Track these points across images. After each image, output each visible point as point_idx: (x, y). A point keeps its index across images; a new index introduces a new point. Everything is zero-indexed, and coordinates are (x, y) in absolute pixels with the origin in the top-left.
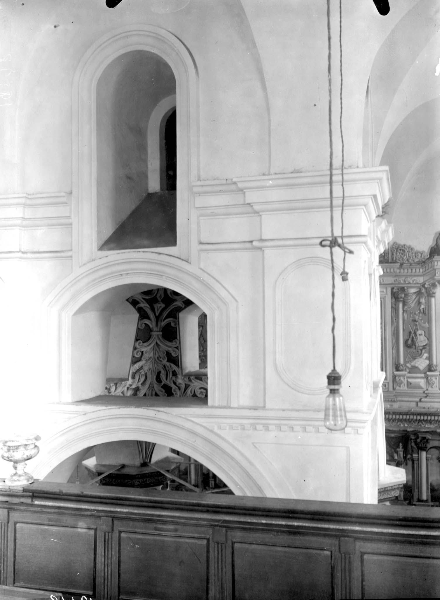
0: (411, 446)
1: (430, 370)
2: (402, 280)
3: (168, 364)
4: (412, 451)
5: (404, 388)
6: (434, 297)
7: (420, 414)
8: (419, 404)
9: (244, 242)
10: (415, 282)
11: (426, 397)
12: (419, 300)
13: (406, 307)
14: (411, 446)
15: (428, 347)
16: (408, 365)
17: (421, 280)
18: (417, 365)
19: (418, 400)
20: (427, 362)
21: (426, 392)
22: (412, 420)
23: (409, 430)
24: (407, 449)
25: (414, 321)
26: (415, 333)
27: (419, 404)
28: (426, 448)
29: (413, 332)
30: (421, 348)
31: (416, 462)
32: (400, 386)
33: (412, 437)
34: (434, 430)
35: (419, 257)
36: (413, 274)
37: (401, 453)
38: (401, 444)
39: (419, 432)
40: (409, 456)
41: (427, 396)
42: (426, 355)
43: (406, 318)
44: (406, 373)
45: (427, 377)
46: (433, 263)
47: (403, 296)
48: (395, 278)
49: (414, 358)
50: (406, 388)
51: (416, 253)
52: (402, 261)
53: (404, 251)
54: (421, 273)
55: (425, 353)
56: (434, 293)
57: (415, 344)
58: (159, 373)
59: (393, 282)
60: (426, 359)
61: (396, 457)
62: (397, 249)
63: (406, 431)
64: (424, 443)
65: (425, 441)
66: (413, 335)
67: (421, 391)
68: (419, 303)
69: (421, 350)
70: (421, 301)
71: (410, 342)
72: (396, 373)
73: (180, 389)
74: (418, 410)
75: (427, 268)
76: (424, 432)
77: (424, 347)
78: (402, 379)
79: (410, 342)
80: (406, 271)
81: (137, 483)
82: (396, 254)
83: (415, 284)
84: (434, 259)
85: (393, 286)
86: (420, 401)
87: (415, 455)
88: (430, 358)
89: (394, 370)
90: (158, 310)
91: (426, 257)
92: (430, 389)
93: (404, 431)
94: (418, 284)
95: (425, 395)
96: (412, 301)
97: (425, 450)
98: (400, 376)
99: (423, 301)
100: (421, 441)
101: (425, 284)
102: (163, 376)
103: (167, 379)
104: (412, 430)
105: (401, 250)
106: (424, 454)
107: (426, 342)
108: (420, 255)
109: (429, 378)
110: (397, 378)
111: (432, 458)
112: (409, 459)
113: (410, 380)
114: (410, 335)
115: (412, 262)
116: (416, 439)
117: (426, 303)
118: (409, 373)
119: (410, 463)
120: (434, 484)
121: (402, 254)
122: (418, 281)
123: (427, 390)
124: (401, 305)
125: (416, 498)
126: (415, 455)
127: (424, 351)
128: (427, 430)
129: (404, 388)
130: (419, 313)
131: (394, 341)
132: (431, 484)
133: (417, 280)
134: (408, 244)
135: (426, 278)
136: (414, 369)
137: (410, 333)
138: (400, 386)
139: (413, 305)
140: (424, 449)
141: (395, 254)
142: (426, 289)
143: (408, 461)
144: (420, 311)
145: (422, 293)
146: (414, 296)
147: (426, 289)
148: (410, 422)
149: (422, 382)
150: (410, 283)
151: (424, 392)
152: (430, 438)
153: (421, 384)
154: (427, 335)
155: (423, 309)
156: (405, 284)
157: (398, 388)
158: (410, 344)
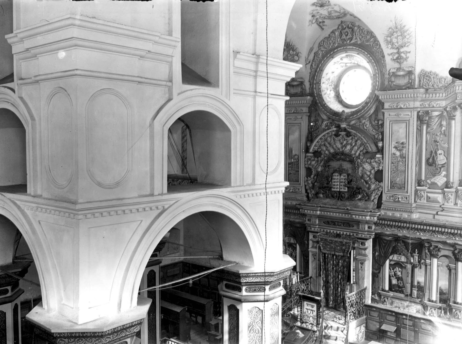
0: (425, 253)
1: (447, 187)
2: (426, 104)
4: (426, 257)
5: (424, 201)
6: (454, 119)
7: (436, 226)
8: (436, 216)
9: (229, 74)
10: (438, 106)
11: (442, 211)
12: (441, 122)
13: (429, 129)
14: (425, 253)
15: (446, 166)
16: (428, 181)
17: (443, 104)
18: (436, 181)
19: (435, 213)
20: (445, 179)
21: (442, 206)
22: (444, 232)
23: (423, 238)
24: (421, 254)
25: (436, 141)
26: (436, 153)
27: (436, 216)
28: (438, 255)
29: (434, 152)
30: (440, 166)
31: (428, 267)
32: (420, 200)
33: (427, 245)
34: (444, 240)
35: (443, 82)
36: (436, 98)
37: (417, 258)
38: (417, 250)
39: (432, 241)
40: (423, 261)
41: (443, 210)
42: (444, 173)
43: (428, 138)
44: (426, 188)
45: (444, 193)
46: (455, 87)
47: (427, 118)
48: (421, 103)
49: (434, 176)
50: (425, 201)
51: (440, 79)
52: (428, 87)
53: (430, 77)
54: (444, 97)
55: (443, 171)
56: (455, 116)
57: (435, 162)
60: (444, 177)
61: (412, 261)
62: (424, 76)
63: (421, 239)
64: (436, 251)
65: (437, 249)
66: (433, 154)
67: (438, 205)
68: (441, 125)
69: (440, 168)
70: (443, 123)
71: (431, 160)
72: (418, 187)
74: (434, 222)
75: (449, 93)
76: (436, 242)
77: (443, 166)
78: (422, 193)
79: (431, 160)
80: (431, 95)
82: (423, 80)
83: (438, 107)
84: (456, 84)
85: (419, 109)
86: (437, 214)
87: (428, 261)
88: (447, 176)
89: (417, 185)
91: (449, 82)
92: (446, 204)
93: (419, 238)
94: (440, 107)
95: (441, 209)
96: (435, 123)
97: (437, 258)
98: (421, 190)
99: (444, 123)
100: (434, 249)
101: (447, 107)
104: (426, 238)
105: (427, 76)
106: (435, 261)
107: (445, 161)
108: (443, 80)
109: (446, 194)
110: (418, 192)
111: (442, 266)
112: (422, 264)
113: (429, 195)
114: (431, 155)
115: (437, 87)
116: (429, 247)
117: (447, 125)
118: (429, 188)
119: (423, 267)
120: (443, 288)
121: (428, 80)
122: (441, 105)
123: (443, 204)
124: (425, 127)
125: (452, 299)
126: (428, 261)
127: (442, 169)
128: (439, 240)
129: (424, 201)
130: (440, 134)
131: (418, 159)
132: (440, 288)
134: (433, 71)
135: (448, 102)
136: (433, 185)
137: (432, 152)
138: (420, 200)
139: (435, 127)
140: (435, 256)
141: (422, 80)
142: (447, 112)
143: (422, 265)
144: (441, 132)
145: (444, 116)
146: (437, 119)
147: (447, 112)
148: (425, 232)
149: (440, 197)
150: (433, 107)
151: (440, 206)
152: (442, 247)
153: (438, 199)
154: (446, 155)
155: (444, 130)
156: (429, 108)
157: (418, 201)
158: (431, 162)
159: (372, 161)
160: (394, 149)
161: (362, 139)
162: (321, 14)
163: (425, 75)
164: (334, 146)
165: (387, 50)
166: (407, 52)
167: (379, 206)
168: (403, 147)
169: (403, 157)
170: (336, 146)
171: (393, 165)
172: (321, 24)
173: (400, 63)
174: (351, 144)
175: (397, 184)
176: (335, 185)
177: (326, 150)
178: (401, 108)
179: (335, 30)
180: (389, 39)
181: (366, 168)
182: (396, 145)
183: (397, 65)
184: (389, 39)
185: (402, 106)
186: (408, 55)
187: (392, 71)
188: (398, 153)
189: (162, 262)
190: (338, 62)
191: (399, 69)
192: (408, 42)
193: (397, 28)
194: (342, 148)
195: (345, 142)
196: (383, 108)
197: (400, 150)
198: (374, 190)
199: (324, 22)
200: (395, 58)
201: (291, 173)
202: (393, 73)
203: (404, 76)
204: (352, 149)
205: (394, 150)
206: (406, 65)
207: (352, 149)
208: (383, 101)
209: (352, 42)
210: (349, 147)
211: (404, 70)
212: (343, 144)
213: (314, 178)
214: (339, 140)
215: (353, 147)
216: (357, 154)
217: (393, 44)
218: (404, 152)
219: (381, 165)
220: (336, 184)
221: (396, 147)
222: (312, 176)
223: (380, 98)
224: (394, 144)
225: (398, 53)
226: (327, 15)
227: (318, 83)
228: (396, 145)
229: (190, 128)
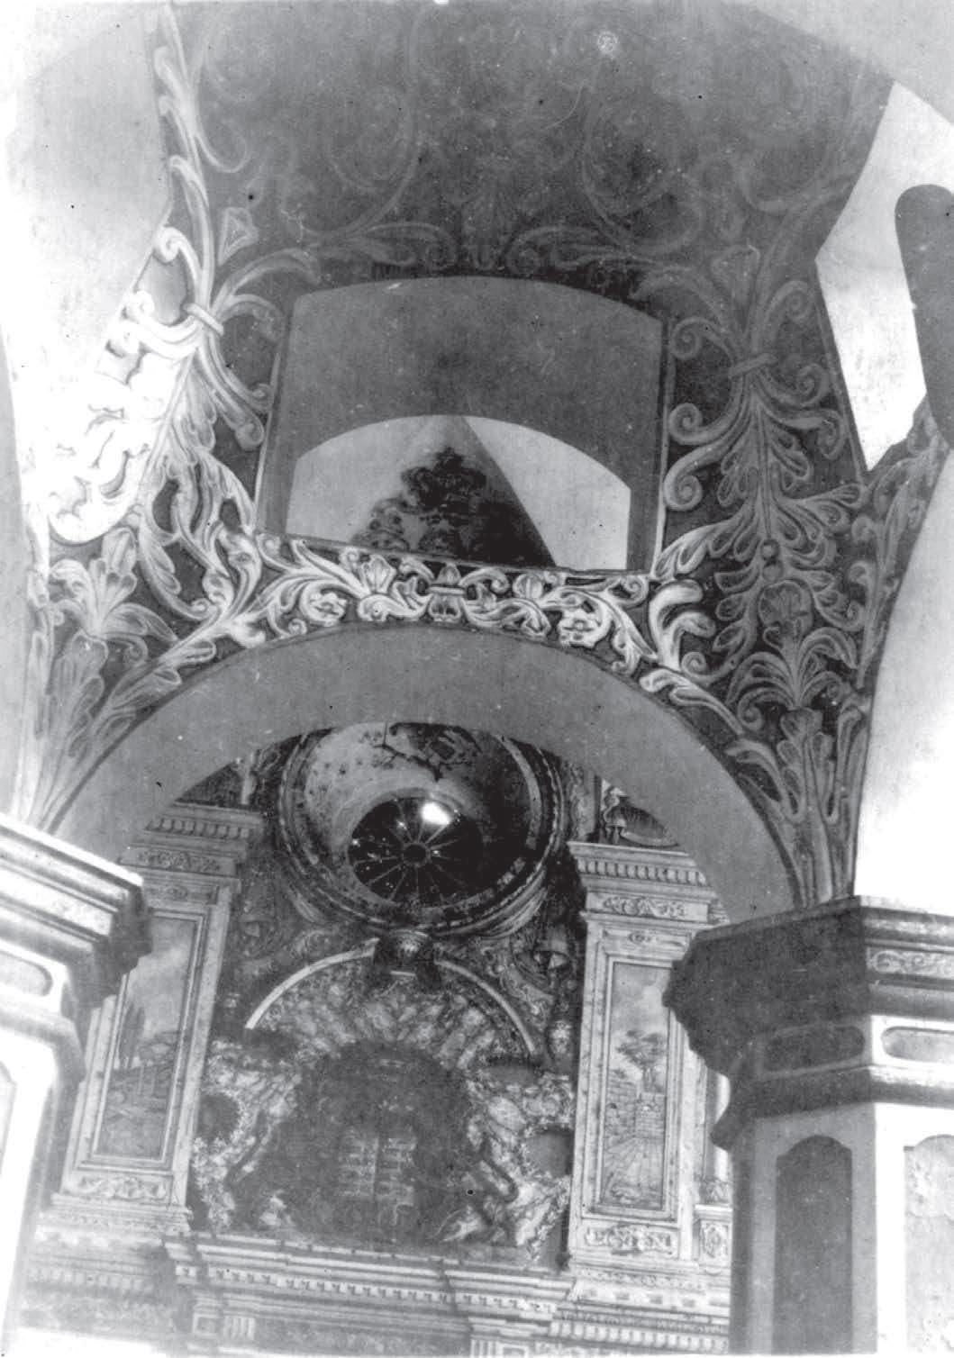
3: (213, 465)
58: (172, 487)
59: (475, 734)
72: (701, 1208)
73: (236, 586)
81: (835, 373)
89: (698, 1198)
90: (230, 242)
102: (183, 511)
103: (194, 526)
133: (531, 1219)
138: (712, 1256)
160: (621, 1056)
164: (360, 1022)
167: (560, 1259)
168: (654, 1052)
171: (612, 1112)
175: (627, 1185)
178: (649, 916)
181: (500, 1119)
182: (629, 1041)
185: (656, 913)
188: (635, 1074)
189: (389, 486)
194: (395, 1031)
197: (644, 1064)
201: (118, 1117)
205: (619, 1061)
212: (403, 1018)
213: (242, 1142)
216: (463, 1061)
218: (660, 1068)
219: (569, 1110)
220: (360, 1171)
221: (627, 1051)
222: (236, 1135)
228: (629, 1041)
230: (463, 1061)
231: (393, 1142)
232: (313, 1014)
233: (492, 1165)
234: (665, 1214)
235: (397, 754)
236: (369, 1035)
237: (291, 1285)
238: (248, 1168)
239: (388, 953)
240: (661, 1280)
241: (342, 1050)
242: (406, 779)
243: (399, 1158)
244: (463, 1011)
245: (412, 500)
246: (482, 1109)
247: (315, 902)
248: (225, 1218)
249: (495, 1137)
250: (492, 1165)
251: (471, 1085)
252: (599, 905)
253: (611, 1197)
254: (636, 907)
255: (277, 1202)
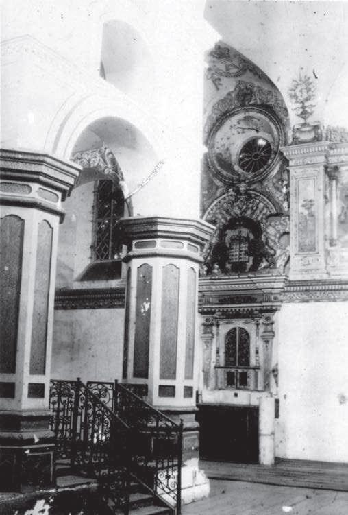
159: (277, 223)
161: (265, 200)
162: (218, 69)
163: (331, 131)
164: (232, 213)
165: (292, 107)
166: (312, 106)
169: (312, 215)
170: (234, 212)
172: (217, 83)
173: (305, 118)
174: (252, 208)
175: (305, 245)
176: (233, 255)
177: (222, 218)
179: (232, 92)
180: (293, 93)
182: (304, 203)
183: (302, 121)
184: (293, 93)
185: (309, 162)
186: (313, 109)
187: (295, 127)
190: (235, 125)
191: (304, 125)
192: (313, 95)
193: (301, 80)
194: (241, 213)
195: (244, 207)
196: (288, 165)
197: (308, 209)
198: (280, 256)
199: (220, 79)
200: (299, 113)
202: (298, 129)
203: (309, 131)
204: (253, 213)
205: (301, 210)
206: (311, 120)
207: (253, 213)
208: (288, 158)
209: (251, 103)
210: (249, 212)
211: (309, 125)
213: (206, 252)
214: (238, 205)
215: (255, 211)
216: (259, 219)
217: (297, 97)
218: (313, 209)
220: (234, 254)
221: (303, 206)
223: (285, 154)
224: (301, 202)
225: (303, 107)
226: (225, 70)
227: (174, 310)
229: (158, 216)
230: (259, 219)
231: (242, 245)
232: (220, 213)
233: (269, 246)
234: (316, 252)
235: (244, 129)
236: (235, 215)
237: (206, 288)
238: (209, 258)
239: (238, 192)
240: (313, 271)
241: (229, 222)
242: (253, 134)
243: (243, 249)
244: (258, 204)
245: (215, 60)
246: (265, 231)
247: (221, 180)
248: (205, 273)
249: (269, 238)
250: (269, 246)
251: (262, 225)
252: (293, 164)
253: (302, 248)
254: (303, 162)
255: (216, 266)
